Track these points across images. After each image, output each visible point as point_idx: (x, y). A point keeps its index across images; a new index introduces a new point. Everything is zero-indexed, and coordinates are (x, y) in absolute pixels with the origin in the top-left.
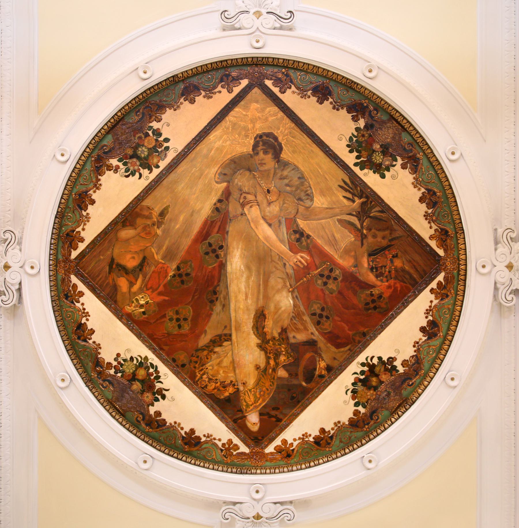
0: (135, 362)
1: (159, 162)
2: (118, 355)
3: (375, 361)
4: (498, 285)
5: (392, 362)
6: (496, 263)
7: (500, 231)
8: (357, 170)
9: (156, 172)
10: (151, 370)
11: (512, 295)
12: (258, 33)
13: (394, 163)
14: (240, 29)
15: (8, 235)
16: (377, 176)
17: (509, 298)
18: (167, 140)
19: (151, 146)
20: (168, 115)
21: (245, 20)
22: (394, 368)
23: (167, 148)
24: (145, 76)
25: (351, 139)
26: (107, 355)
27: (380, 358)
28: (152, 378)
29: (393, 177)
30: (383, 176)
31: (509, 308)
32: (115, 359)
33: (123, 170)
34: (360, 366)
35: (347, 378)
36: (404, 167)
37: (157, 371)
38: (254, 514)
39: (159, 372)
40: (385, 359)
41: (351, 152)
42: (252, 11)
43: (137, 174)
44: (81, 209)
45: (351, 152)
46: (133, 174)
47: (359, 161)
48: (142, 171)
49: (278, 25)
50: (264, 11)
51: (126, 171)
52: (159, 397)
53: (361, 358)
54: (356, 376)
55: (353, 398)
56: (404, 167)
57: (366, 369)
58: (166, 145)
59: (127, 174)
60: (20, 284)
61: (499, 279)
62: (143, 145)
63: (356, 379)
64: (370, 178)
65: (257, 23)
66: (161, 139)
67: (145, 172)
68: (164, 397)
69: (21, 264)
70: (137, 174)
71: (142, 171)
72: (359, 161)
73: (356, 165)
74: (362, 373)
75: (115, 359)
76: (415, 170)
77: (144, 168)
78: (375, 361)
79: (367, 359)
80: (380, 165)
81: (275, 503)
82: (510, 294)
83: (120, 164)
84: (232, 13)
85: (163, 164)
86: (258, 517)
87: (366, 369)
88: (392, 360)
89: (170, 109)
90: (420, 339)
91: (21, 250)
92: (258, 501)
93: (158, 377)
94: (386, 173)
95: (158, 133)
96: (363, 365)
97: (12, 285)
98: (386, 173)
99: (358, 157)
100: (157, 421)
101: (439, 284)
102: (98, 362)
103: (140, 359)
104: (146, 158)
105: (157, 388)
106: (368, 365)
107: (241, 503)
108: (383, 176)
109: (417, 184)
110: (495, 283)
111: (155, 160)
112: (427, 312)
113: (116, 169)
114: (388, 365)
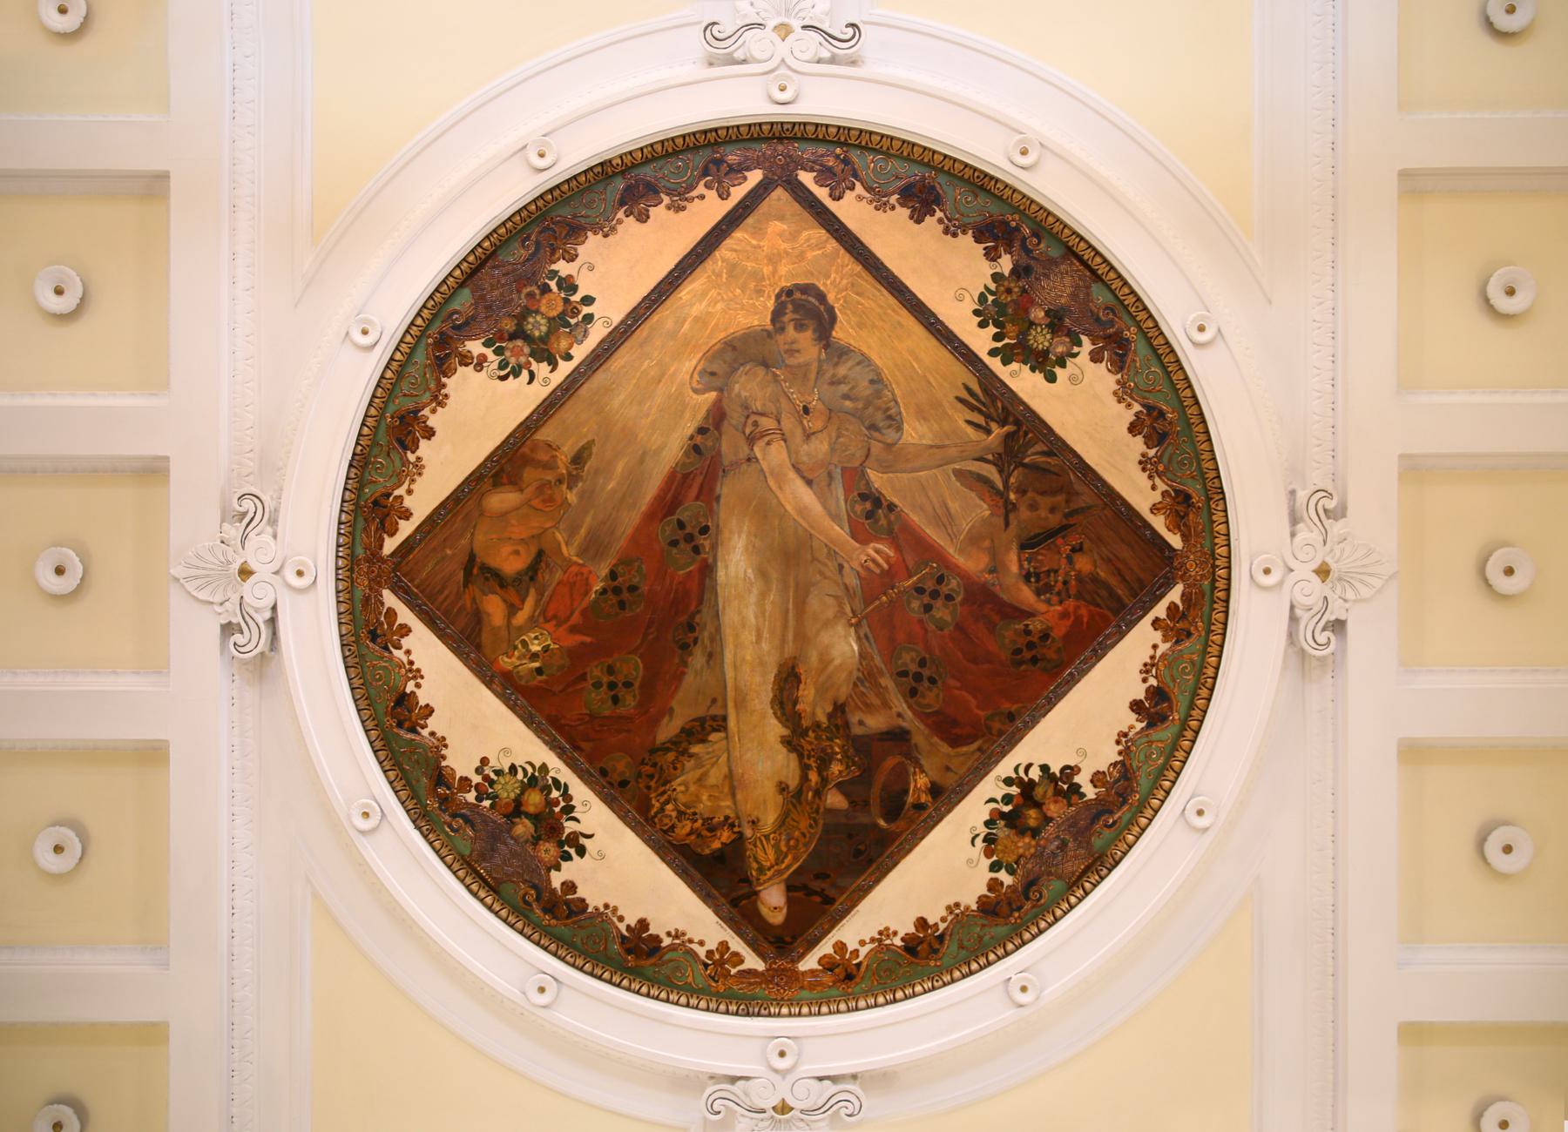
0: (520, 775)
1: (571, 346)
2: (484, 761)
3: (1035, 774)
4: (1298, 612)
5: (1071, 776)
6: (1292, 563)
7: (1302, 495)
8: (995, 364)
9: (565, 368)
10: (555, 794)
11: (1328, 634)
12: (783, 71)
13: (1076, 349)
14: (744, 62)
15: (248, 505)
16: (1039, 377)
17: (1322, 639)
18: (588, 300)
19: (554, 314)
20: (590, 246)
21: (755, 43)
22: (1075, 788)
23: (589, 318)
24: (542, 163)
25: (982, 298)
26: (461, 762)
27: (1045, 768)
28: (557, 809)
29: (1073, 380)
30: (1051, 378)
31: (1322, 660)
32: (478, 771)
33: (495, 365)
34: (1002, 784)
35: (973, 811)
36: (1096, 357)
37: (567, 796)
38: (775, 1101)
39: (571, 799)
40: (1055, 769)
41: (982, 325)
42: (771, 24)
43: (525, 374)
44: (405, 448)
45: (982, 325)
46: (516, 373)
47: (999, 345)
48: (534, 366)
49: (826, 54)
50: (796, 24)
51: (502, 366)
52: (572, 851)
53: (1005, 768)
54: (993, 805)
55: (988, 853)
56: (1096, 357)
57: (1014, 790)
58: (586, 310)
59: (503, 373)
60: (274, 608)
61: (1301, 599)
62: (537, 312)
63: (993, 811)
64: (1023, 381)
65: (782, 49)
66: (576, 298)
67: (542, 369)
68: (582, 851)
69: (275, 566)
70: (525, 374)
71: (534, 366)
72: (999, 345)
73: (993, 353)
74: (1007, 799)
75: (478, 771)
76: (1119, 365)
77: (539, 361)
78: (1035, 774)
79: (1016, 769)
80: (1045, 353)
81: (821, 1079)
82: (1324, 629)
83: (489, 352)
84: (727, 27)
85: (580, 352)
86: (783, 1108)
87: (1014, 790)
88: (1070, 771)
89: (595, 233)
90: (1131, 727)
91: (275, 537)
92: (783, 1073)
93: (569, 809)
94: (1057, 370)
95: (569, 285)
96: (1008, 782)
97: (257, 610)
98: (1057, 370)
99: (997, 338)
100: (567, 903)
101: (1172, 608)
102: (440, 777)
103: (530, 770)
104: (544, 339)
105: (567, 831)
106: (1019, 782)
107: (747, 1078)
108: (1051, 378)
109: (1123, 394)
110: (1292, 607)
111: (564, 344)
112: (1146, 669)
113: (480, 364)
114: (1062, 782)
